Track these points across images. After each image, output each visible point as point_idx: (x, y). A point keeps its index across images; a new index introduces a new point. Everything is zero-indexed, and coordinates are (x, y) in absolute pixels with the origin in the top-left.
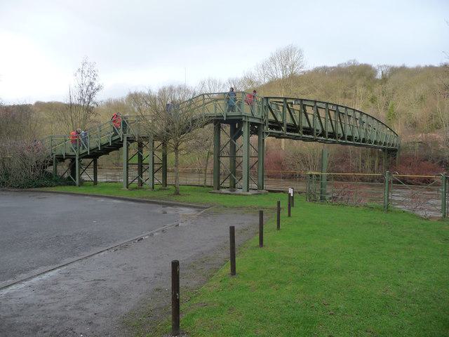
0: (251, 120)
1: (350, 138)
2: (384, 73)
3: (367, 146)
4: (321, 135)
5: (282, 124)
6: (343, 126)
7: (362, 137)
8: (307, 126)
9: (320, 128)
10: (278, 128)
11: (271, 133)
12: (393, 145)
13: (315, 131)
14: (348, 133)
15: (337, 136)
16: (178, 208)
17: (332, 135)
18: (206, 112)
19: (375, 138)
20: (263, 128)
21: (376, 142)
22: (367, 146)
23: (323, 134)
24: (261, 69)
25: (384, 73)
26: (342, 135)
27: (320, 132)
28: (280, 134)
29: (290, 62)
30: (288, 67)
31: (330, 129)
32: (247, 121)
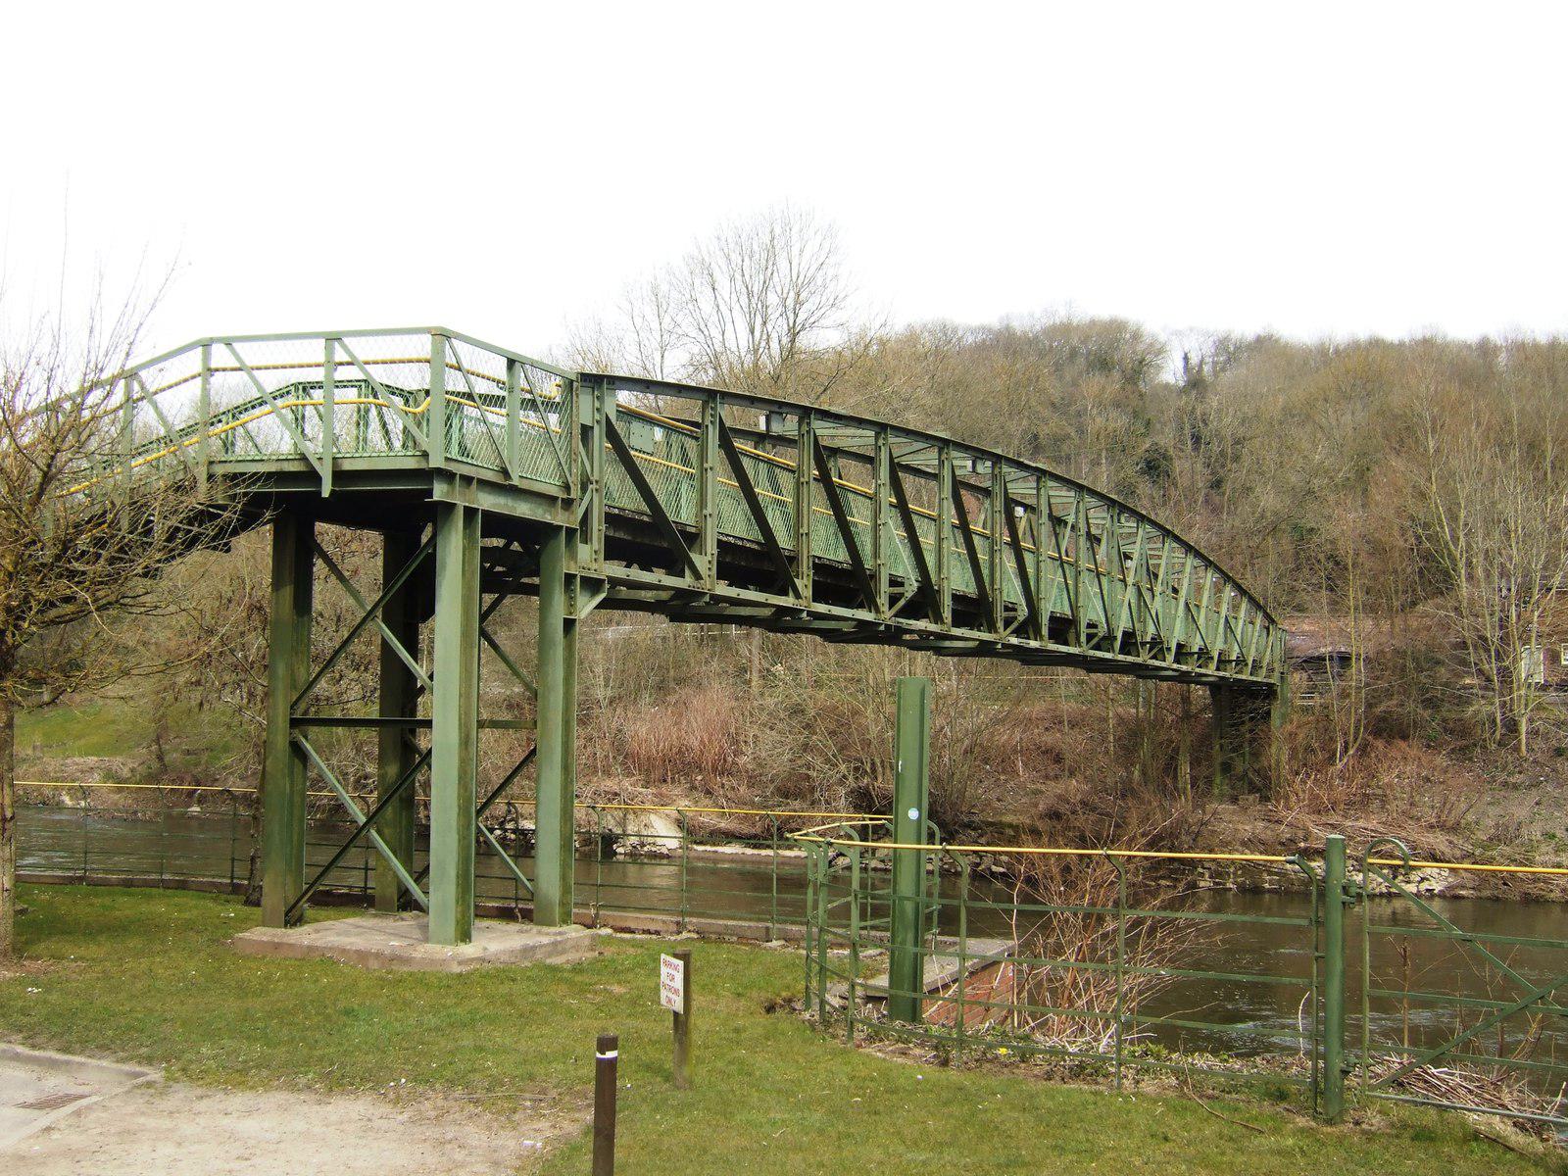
0: (487, 502)
1: (1062, 628)
2: (1194, 360)
3: (1140, 671)
4: (913, 609)
5: (694, 538)
6: (983, 557)
7: (1123, 624)
8: (840, 555)
9: (906, 569)
10: (781, 583)
11: (614, 582)
12: (1256, 666)
13: (884, 588)
14: (1054, 603)
15: (1000, 614)
16: (913, 930)
17: (974, 610)
18: (242, 448)
19: (1176, 634)
20: (573, 554)
21: (1182, 652)
22: (1140, 671)
23: (924, 602)
24: (650, 311)
25: (1194, 360)
26: (1023, 612)
27: (911, 588)
28: (781, 611)
29: (782, 278)
30: (773, 299)
31: (957, 580)
32: (461, 502)
